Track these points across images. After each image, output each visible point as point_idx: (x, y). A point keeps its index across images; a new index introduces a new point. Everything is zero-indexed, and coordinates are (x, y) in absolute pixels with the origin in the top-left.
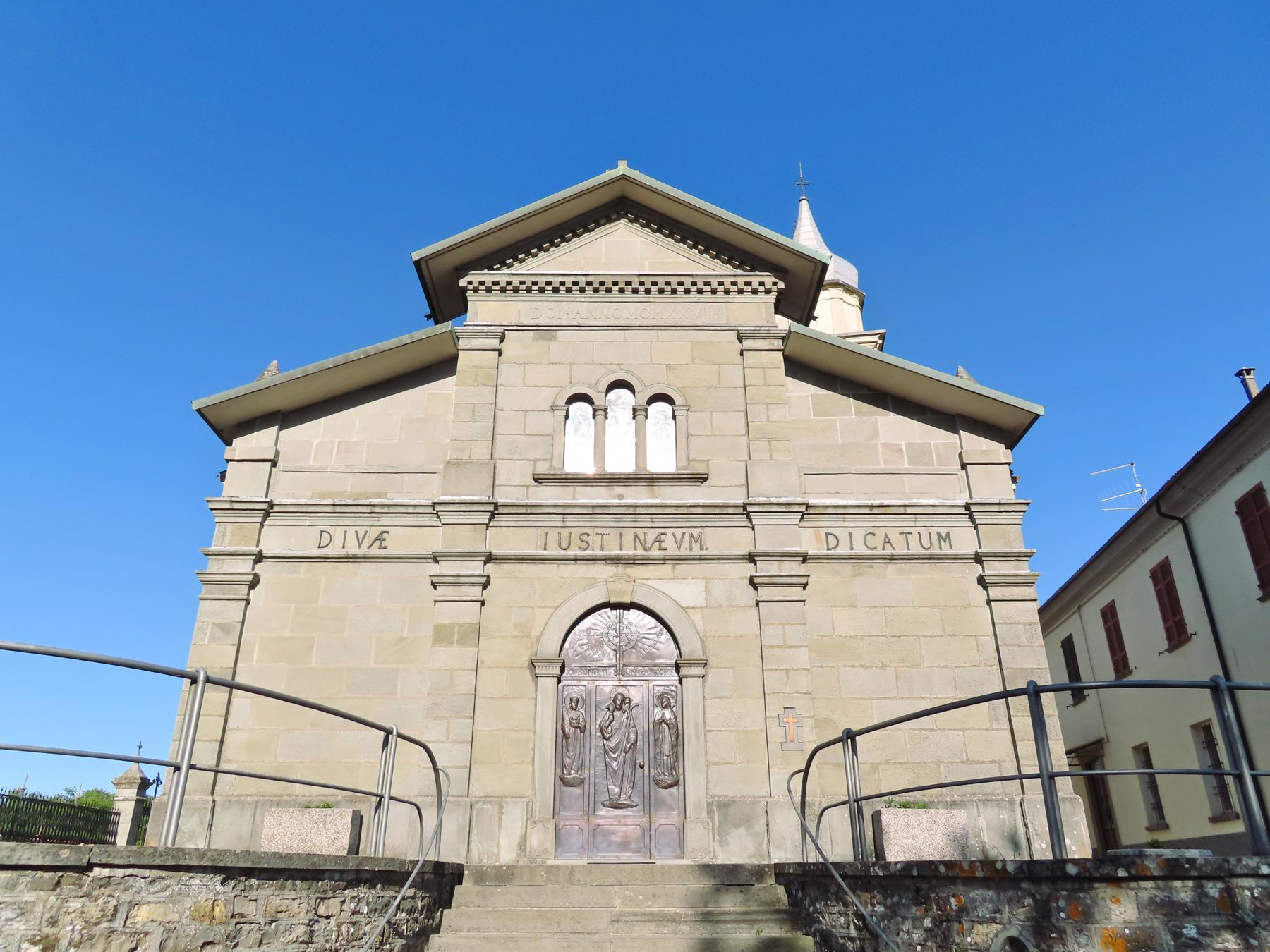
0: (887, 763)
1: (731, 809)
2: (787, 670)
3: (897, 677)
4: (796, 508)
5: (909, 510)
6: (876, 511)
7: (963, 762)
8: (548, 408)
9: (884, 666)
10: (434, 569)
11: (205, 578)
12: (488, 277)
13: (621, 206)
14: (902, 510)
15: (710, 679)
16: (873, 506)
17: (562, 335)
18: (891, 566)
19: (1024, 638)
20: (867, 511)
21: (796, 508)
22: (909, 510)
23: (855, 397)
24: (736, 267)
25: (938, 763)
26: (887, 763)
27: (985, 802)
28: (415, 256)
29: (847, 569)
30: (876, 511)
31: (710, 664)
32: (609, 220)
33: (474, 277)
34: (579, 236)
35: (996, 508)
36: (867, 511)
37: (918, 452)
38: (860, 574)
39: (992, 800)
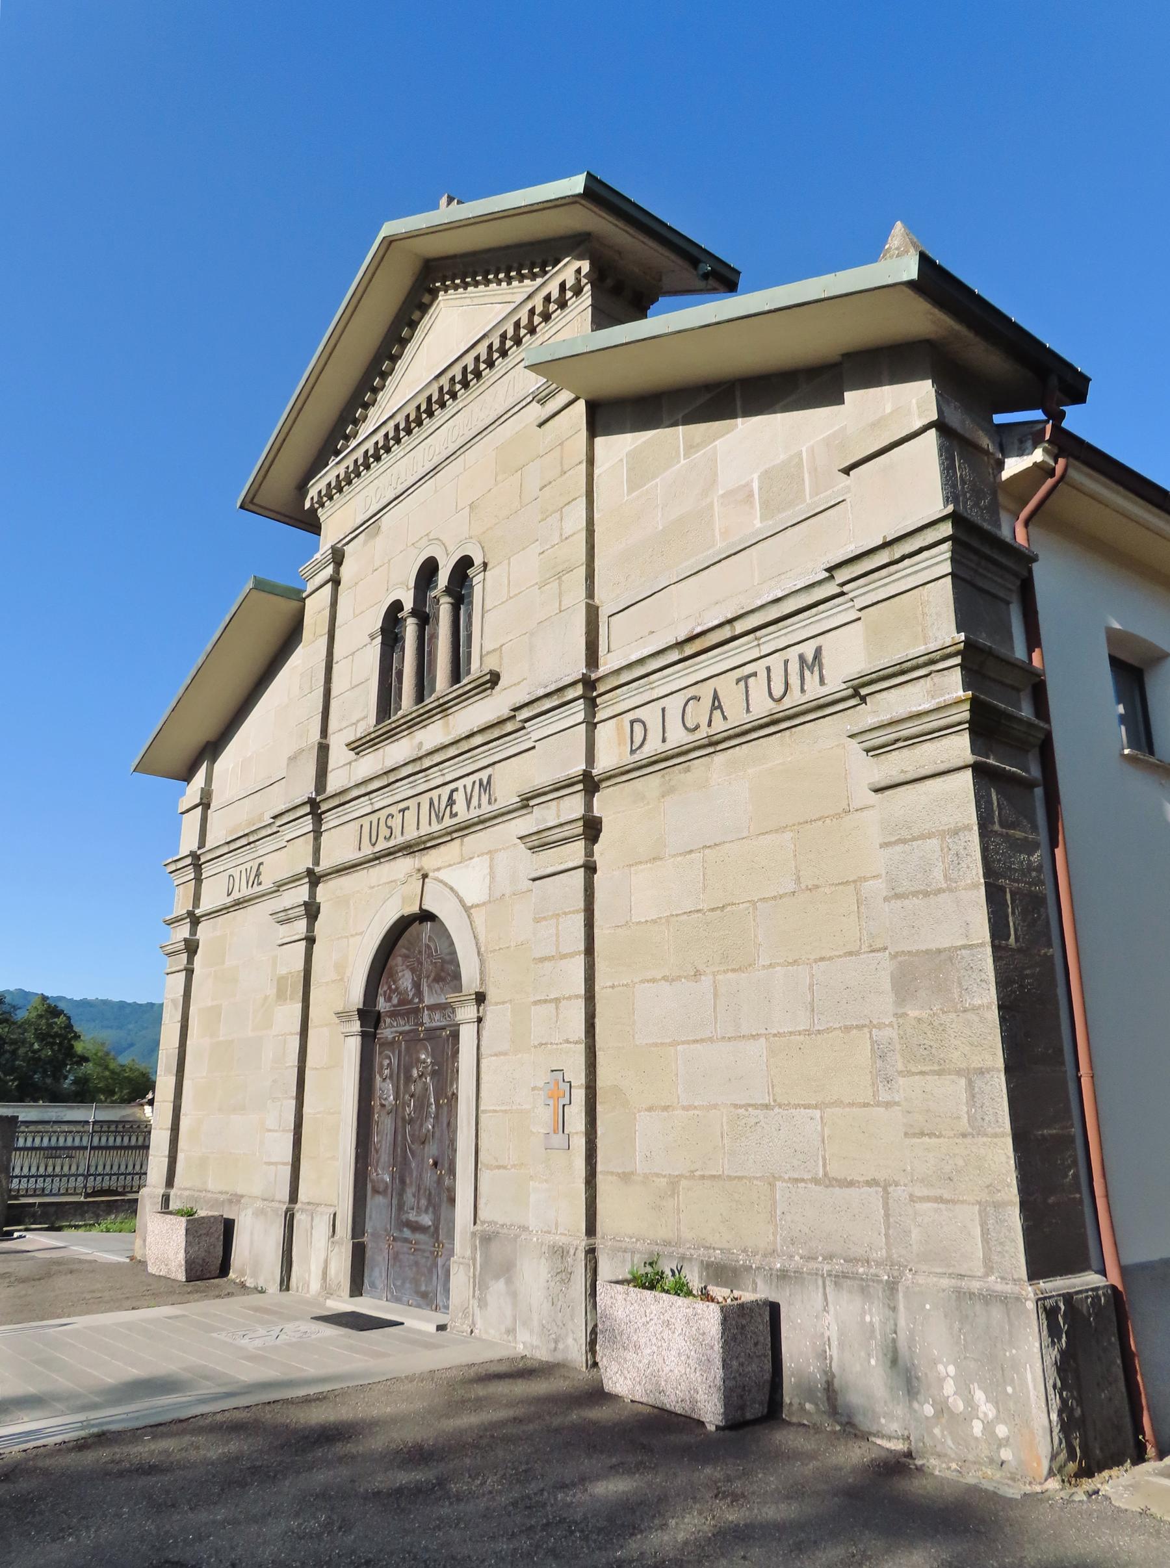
0: (691, 1176)
1: (494, 1247)
2: (557, 1000)
3: (716, 995)
4: (571, 694)
5: (740, 627)
6: (689, 650)
7: (816, 1181)
8: (369, 640)
9: (697, 974)
10: (525, 824)
11: (169, 949)
12: (333, 471)
13: (438, 272)
14: (726, 633)
15: (487, 1023)
16: (679, 645)
17: (387, 520)
18: (719, 758)
19: (938, 874)
20: (675, 656)
21: (571, 694)
22: (740, 627)
23: (688, 420)
24: (534, 277)
25: (771, 1181)
26: (691, 1176)
27: (839, 1279)
28: (238, 504)
29: (652, 784)
30: (689, 650)
31: (491, 997)
32: (424, 308)
33: (316, 487)
34: (399, 357)
35: (883, 558)
36: (675, 656)
37: (781, 480)
38: (672, 790)
39: (855, 1277)
